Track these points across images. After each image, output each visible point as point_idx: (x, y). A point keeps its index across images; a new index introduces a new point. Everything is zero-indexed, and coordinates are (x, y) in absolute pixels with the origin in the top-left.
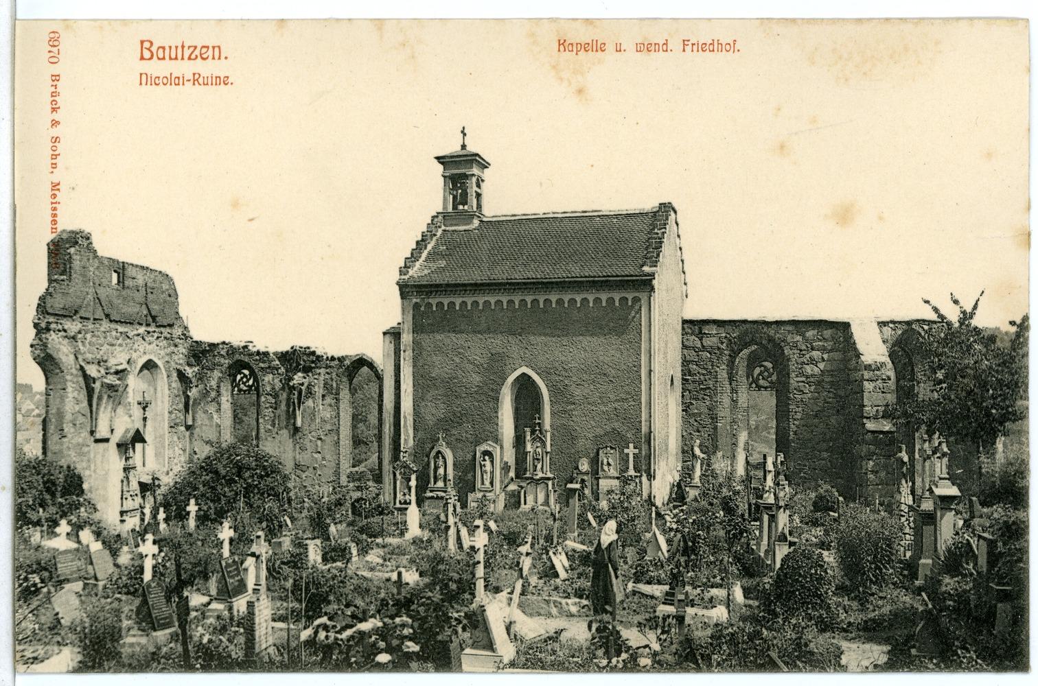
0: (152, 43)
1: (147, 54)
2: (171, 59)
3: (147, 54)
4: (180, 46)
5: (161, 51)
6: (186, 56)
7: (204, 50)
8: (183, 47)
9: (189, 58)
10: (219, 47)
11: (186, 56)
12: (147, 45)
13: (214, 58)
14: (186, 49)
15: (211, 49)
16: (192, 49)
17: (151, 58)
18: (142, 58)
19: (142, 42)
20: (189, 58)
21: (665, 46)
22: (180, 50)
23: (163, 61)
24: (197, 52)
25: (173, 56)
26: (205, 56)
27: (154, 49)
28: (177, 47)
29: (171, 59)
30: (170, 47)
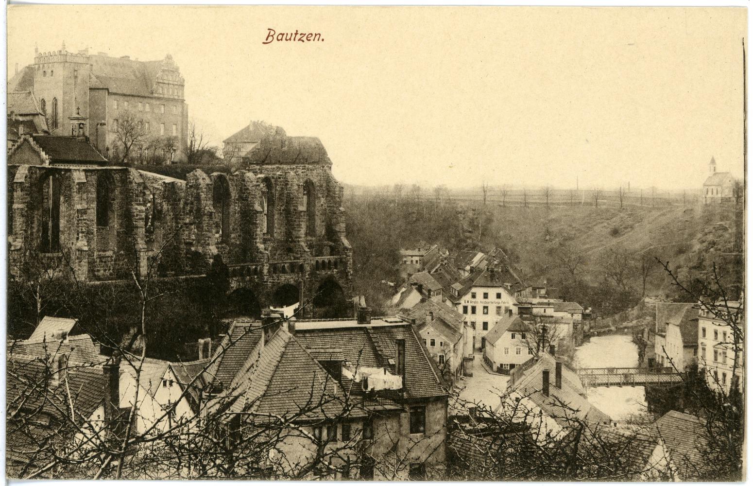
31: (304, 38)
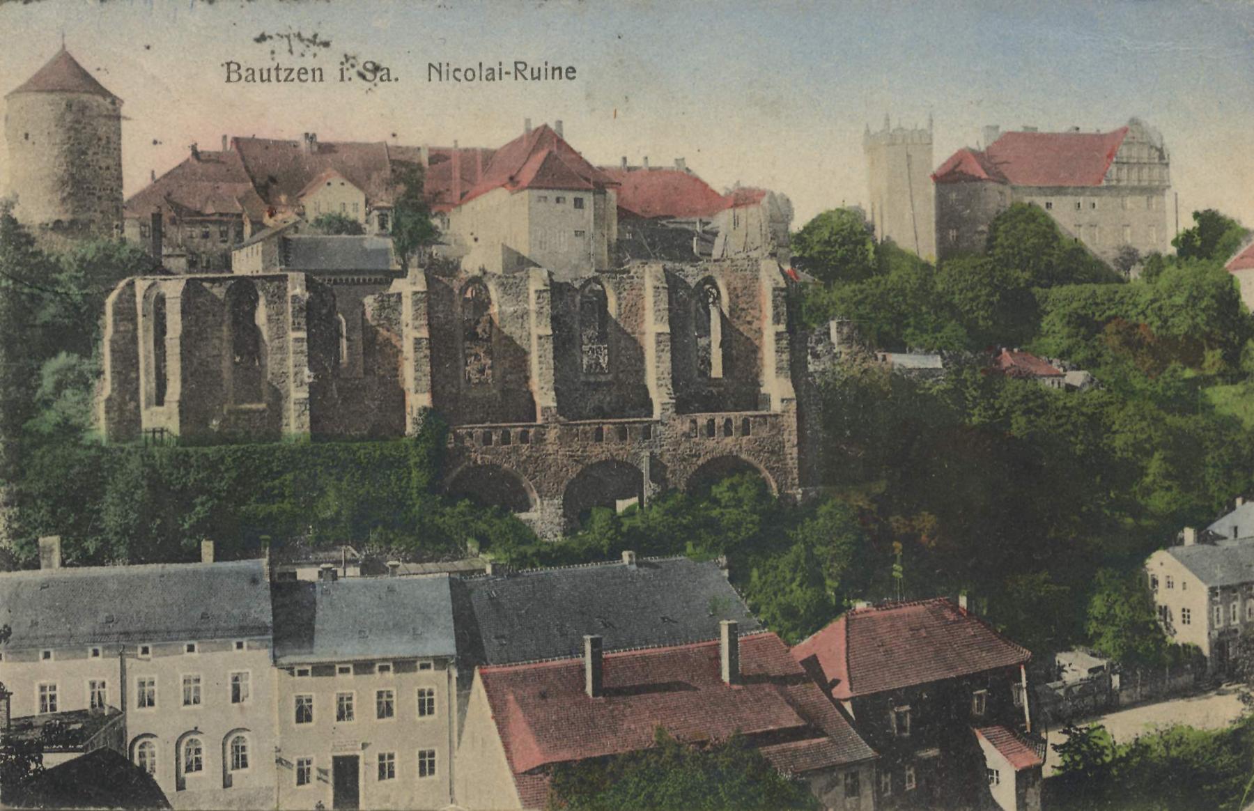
22: (273, 73)
31: (294, 75)
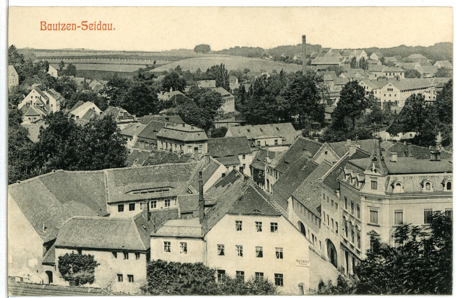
0: (46, 23)
1: (44, 28)
2: (54, 30)
3: (44, 28)
4: (58, 24)
5: (50, 26)
6: (61, 29)
7: (68, 26)
8: (59, 24)
9: (62, 29)
10: (75, 24)
11: (61, 29)
12: (43, 23)
13: (73, 29)
14: (60, 25)
15: (71, 25)
16: (63, 25)
17: (45, 30)
18: (41, 29)
19: (41, 22)
20: (62, 29)
21: (99, 26)
22: (58, 25)
23: (105, 31)
24: (65, 27)
25: (55, 28)
26: (69, 28)
27: (47, 25)
28: (56, 25)
29: (109, 29)
30: (109, 24)
